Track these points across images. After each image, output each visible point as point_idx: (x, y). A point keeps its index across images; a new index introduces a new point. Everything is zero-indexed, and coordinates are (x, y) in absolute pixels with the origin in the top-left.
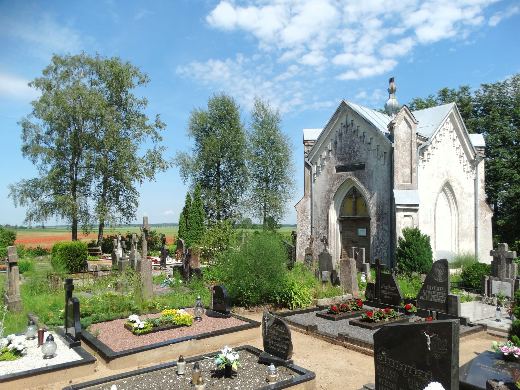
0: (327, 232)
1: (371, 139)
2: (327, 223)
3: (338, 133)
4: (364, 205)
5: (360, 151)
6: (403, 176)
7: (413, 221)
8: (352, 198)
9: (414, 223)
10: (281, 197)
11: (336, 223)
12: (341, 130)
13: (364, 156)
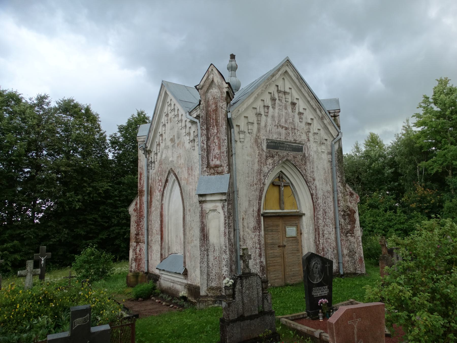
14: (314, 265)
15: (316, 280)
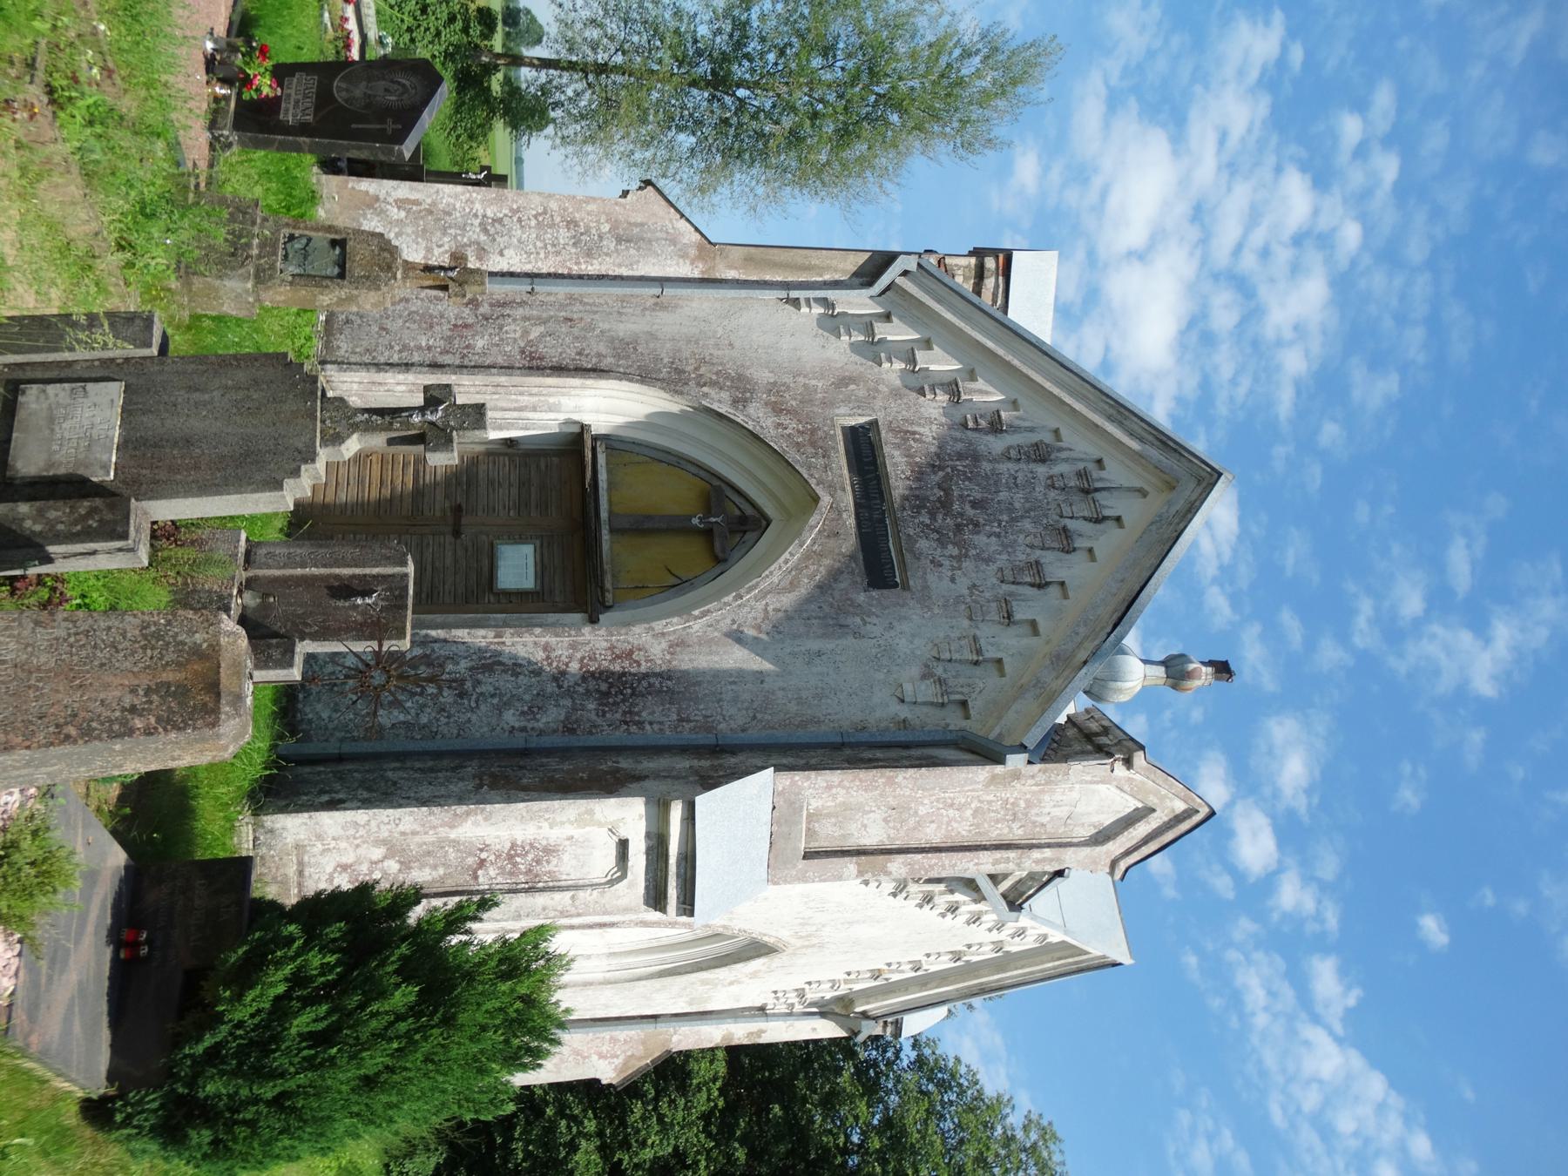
0: (508, 368)
1: (1033, 624)
2: (559, 370)
3: (1048, 438)
4: (674, 581)
5: (967, 564)
6: (845, 812)
7: (593, 886)
8: (708, 511)
9: (581, 894)
10: (646, 145)
11: (562, 417)
12: (1066, 460)
13: (939, 583)
14: (399, 83)
15: (344, 85)
